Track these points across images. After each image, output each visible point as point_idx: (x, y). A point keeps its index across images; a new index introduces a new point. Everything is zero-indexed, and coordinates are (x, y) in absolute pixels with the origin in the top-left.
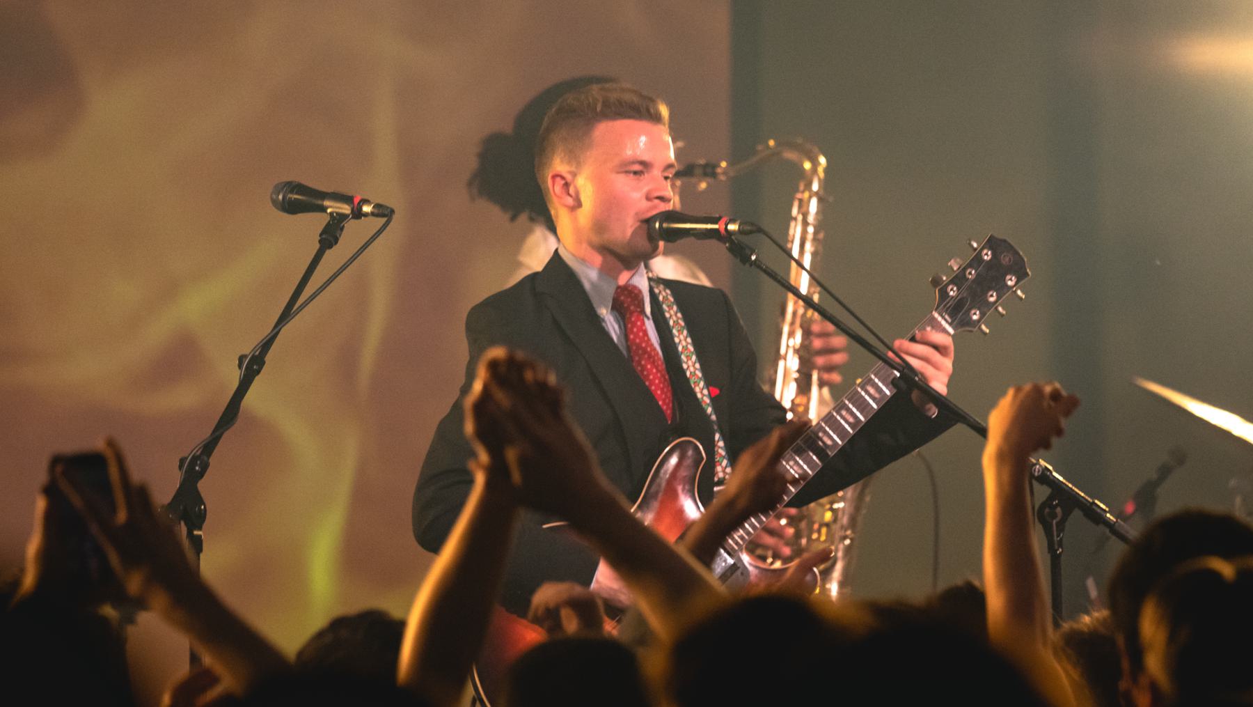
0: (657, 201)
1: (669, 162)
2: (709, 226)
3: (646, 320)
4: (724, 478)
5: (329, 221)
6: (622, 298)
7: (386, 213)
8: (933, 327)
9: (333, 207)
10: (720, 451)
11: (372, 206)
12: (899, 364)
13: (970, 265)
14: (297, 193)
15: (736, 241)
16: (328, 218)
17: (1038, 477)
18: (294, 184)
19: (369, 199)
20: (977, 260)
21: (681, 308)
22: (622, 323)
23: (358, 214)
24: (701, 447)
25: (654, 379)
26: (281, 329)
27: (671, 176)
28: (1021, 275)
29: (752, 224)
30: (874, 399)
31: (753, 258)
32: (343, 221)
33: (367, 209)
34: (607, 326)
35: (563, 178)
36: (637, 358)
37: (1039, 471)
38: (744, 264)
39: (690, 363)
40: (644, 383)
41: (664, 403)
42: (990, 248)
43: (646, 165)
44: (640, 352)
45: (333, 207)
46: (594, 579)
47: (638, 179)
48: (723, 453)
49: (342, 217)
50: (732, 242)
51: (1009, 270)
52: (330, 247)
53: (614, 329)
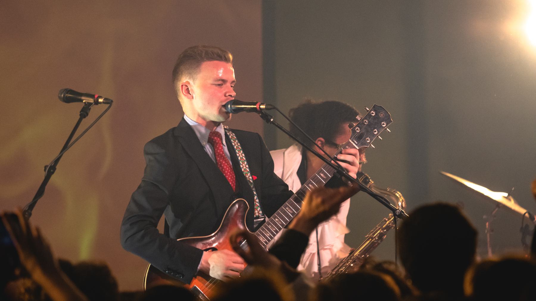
0: (229, 97)
1: (233, 80)
2: (252, 106)
3: (223, 146)
4: (259, 215)
5: (84, 106)
6: (212, 137)
7: (109, 102)
8: (349, 146)
9: (85, 100)
10: (257, 204)
11: (103, 99)
12: (336, 166)
13: (365, 118)
14: (70, 94)
15: (264, 113)
16: (83, 105)
17: (398, 215)
18: (68, 89)
19: (101, 95)
20: (369, 115)
21: (240, 141)
22: (213, 148)
23: (97, 103)
24: (247, 203)
25: (228, 173)
26: (63, 153)
27: (233, 86)
28: (388, 121)
29: (271, 105)
30: (323, 179)
31: (272, 120)
32: (90, 106)
33: (101, 100)
34: (206, 149)
36: (220, 164)
37: (398, 213)
38: (268, 123)
40: (223, 175)
41: (232, 184)
42: (375, 111)
43: (224, 81)
44: (220, 156)
45: (85, 100)
46: (200, 263)
47: (221, 87)
48: (258, 205)
49: (90, 104)
50: (262, 113)
52: (85, 117)
53: (210, 152)
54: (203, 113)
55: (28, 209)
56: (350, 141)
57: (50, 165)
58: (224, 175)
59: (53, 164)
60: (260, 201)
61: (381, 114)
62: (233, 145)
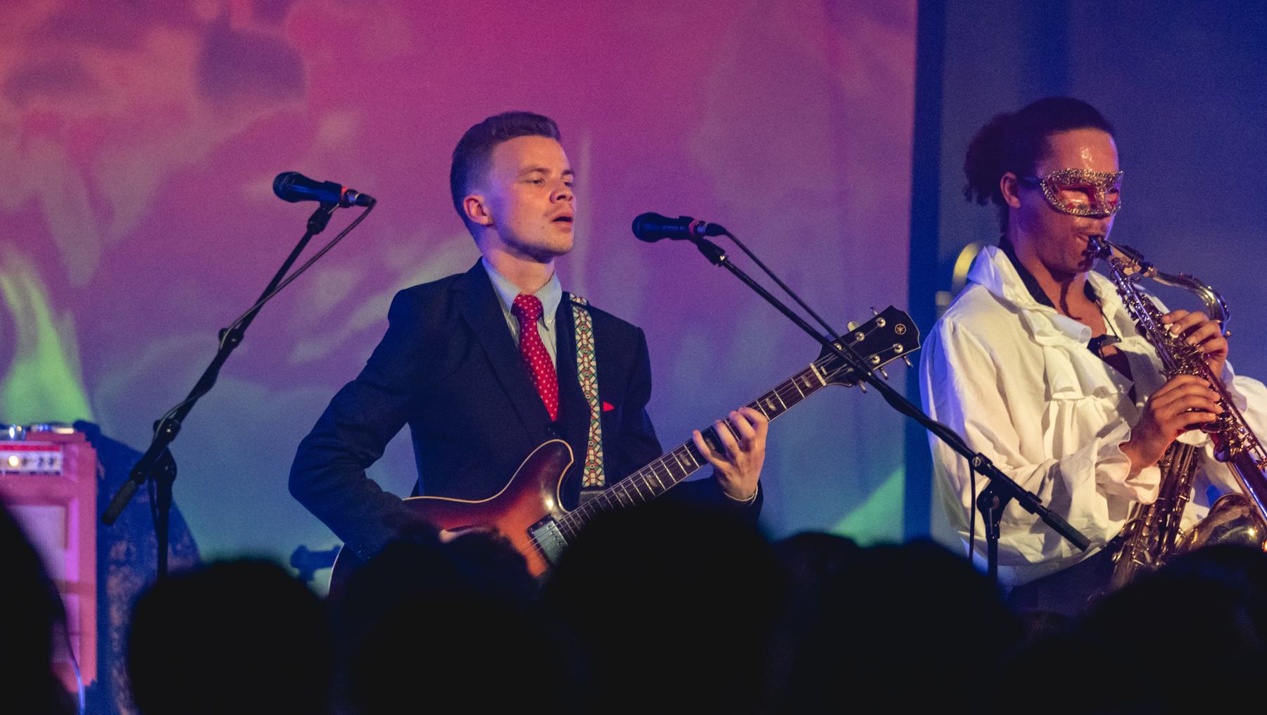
31: (722, 258)
35: (476, 201)
37: (978, 463)
39: (587, 382)
40: (539, 396)
51: (900, 339)
52: (317, 233)
54: (1063, 552)
55: (176, 417)
56: (813, 367)
58: (542, 397)
59: (237, 327)
60: (603, 434)
62: (575, 340)
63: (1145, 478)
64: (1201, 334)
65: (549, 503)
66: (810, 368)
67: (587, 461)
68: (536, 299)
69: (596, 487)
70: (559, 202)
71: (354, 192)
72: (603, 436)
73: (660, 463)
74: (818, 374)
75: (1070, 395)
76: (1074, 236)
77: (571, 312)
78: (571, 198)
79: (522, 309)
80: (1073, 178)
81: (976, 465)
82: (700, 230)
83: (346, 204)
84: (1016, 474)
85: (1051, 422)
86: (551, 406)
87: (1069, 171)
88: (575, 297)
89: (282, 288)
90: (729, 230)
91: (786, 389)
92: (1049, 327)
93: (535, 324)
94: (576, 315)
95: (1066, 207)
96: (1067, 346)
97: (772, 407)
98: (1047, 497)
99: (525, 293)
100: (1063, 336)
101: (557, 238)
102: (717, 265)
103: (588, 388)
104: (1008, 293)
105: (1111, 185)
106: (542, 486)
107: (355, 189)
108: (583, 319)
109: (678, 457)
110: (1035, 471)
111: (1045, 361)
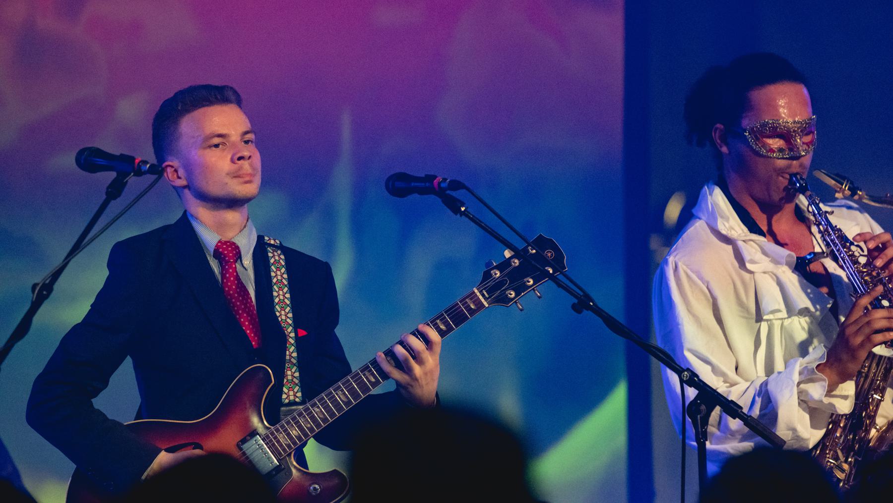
10: (290, 340)
24: (270, 371)
31: (463, 209)
35: (172, 167)
37: (686, 377)
39: (283, 312)
48: (292, 342)
52: (115, 198)
56: (476, 291)
57: (43, 281)
58: (244, 328)
59: (47, 282)
61: (552, 254)
63: (842, 391)
64: (886, 255)
65: (255, 421)
66: (474, 292)
67: (285, 381)
68: (234, 244)
69: (294, 403)
70: (240, 162)
71: (145, 162)
72: (299, 358)
73: (349, 381)
74: (481, 297)
75: (779, 315)
76: (778, 175)
77: (266, 252)
78: (250, 157)
79: (221, 253)
80: (771, 127)
81: (685, 379)
82: (443, 185)
83: (139, 173)
84: (730, 392)
85: (762, 341)
86: (252, 335)
87: (768, 122)
88: (270, 239)
89: (86, 246)
90: (466, 184)
91: (454, 311)
92: (759, 256)
93: (234, 266)
94: (270, 255)
95: (768, 152)
96: (775, 271)
97: (443, 327)
98: (756, 412)
99: (224, 239)
100: (770, 263)
101: (239, 189)
102: (458, 216)
103: (284, 317)
104: (723, 228)
105: (806, 130)
106: (248, 405)
107: (147, 160)
108: (277, 258)
109: (364, 375)
110: (748, 388)
111: (755, 286)
